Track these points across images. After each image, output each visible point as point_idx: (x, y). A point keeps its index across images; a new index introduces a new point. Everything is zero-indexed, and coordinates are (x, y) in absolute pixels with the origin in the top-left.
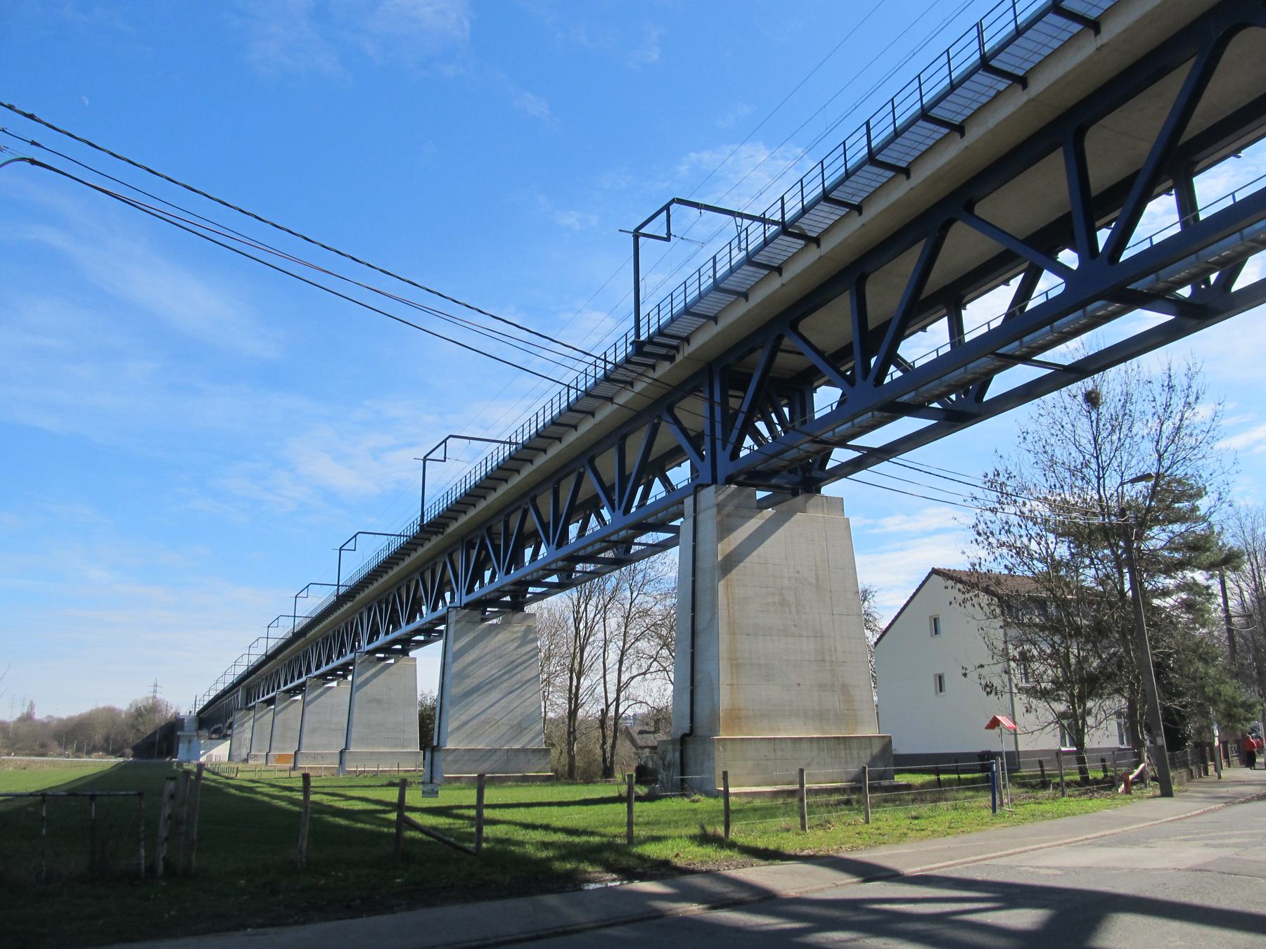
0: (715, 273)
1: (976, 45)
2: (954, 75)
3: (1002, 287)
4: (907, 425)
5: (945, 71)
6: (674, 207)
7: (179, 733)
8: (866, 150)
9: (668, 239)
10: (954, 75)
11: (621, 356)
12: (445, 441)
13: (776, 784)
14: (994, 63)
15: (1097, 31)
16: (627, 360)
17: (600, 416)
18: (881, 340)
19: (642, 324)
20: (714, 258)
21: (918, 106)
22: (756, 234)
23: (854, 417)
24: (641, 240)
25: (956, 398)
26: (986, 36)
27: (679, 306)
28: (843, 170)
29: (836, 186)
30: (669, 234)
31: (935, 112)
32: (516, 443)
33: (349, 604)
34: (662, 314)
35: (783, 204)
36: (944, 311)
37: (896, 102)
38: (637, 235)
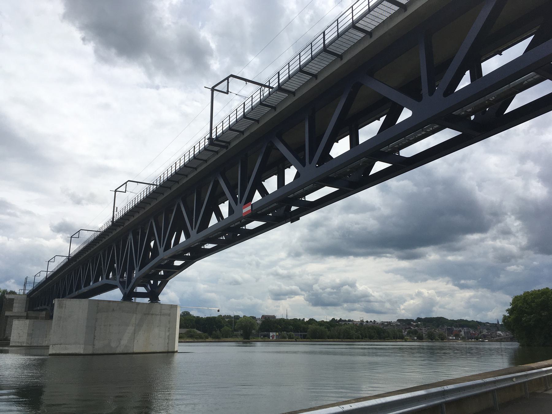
0: (279, 80)
1: (277, 80)
2: (354, 18)
3: (377, 121)
4: (327, 190)
5: (336, 29)
6: (230, 79)
7: (7, 313)
8: (322, 45)
9: (227, 93)
10: (354, 18)
11: (202, 146)
12: (126, 183)
13: (34, 356)
14: (357, 25)
15: (316, 78)
16: (205, 149)
17: (166, 195)
18: (442, 71)
19: (213, 131)
20: (244, 103)
21: (351, 21)
22: (266, 91)
23: (306, 184)
24: (215, 92)
25: (352, 178)
26: (326, 37)
27: (295, 67)
28: (336, 34)
29: (285, 82)
30: (228, 91)
31: (305, 69)
32: (156, 185)
33: (74, 263)
34: (302, 59)
35: (279, 76)
36: (348, 132)
37: (231, 116)
38: (213, 89)
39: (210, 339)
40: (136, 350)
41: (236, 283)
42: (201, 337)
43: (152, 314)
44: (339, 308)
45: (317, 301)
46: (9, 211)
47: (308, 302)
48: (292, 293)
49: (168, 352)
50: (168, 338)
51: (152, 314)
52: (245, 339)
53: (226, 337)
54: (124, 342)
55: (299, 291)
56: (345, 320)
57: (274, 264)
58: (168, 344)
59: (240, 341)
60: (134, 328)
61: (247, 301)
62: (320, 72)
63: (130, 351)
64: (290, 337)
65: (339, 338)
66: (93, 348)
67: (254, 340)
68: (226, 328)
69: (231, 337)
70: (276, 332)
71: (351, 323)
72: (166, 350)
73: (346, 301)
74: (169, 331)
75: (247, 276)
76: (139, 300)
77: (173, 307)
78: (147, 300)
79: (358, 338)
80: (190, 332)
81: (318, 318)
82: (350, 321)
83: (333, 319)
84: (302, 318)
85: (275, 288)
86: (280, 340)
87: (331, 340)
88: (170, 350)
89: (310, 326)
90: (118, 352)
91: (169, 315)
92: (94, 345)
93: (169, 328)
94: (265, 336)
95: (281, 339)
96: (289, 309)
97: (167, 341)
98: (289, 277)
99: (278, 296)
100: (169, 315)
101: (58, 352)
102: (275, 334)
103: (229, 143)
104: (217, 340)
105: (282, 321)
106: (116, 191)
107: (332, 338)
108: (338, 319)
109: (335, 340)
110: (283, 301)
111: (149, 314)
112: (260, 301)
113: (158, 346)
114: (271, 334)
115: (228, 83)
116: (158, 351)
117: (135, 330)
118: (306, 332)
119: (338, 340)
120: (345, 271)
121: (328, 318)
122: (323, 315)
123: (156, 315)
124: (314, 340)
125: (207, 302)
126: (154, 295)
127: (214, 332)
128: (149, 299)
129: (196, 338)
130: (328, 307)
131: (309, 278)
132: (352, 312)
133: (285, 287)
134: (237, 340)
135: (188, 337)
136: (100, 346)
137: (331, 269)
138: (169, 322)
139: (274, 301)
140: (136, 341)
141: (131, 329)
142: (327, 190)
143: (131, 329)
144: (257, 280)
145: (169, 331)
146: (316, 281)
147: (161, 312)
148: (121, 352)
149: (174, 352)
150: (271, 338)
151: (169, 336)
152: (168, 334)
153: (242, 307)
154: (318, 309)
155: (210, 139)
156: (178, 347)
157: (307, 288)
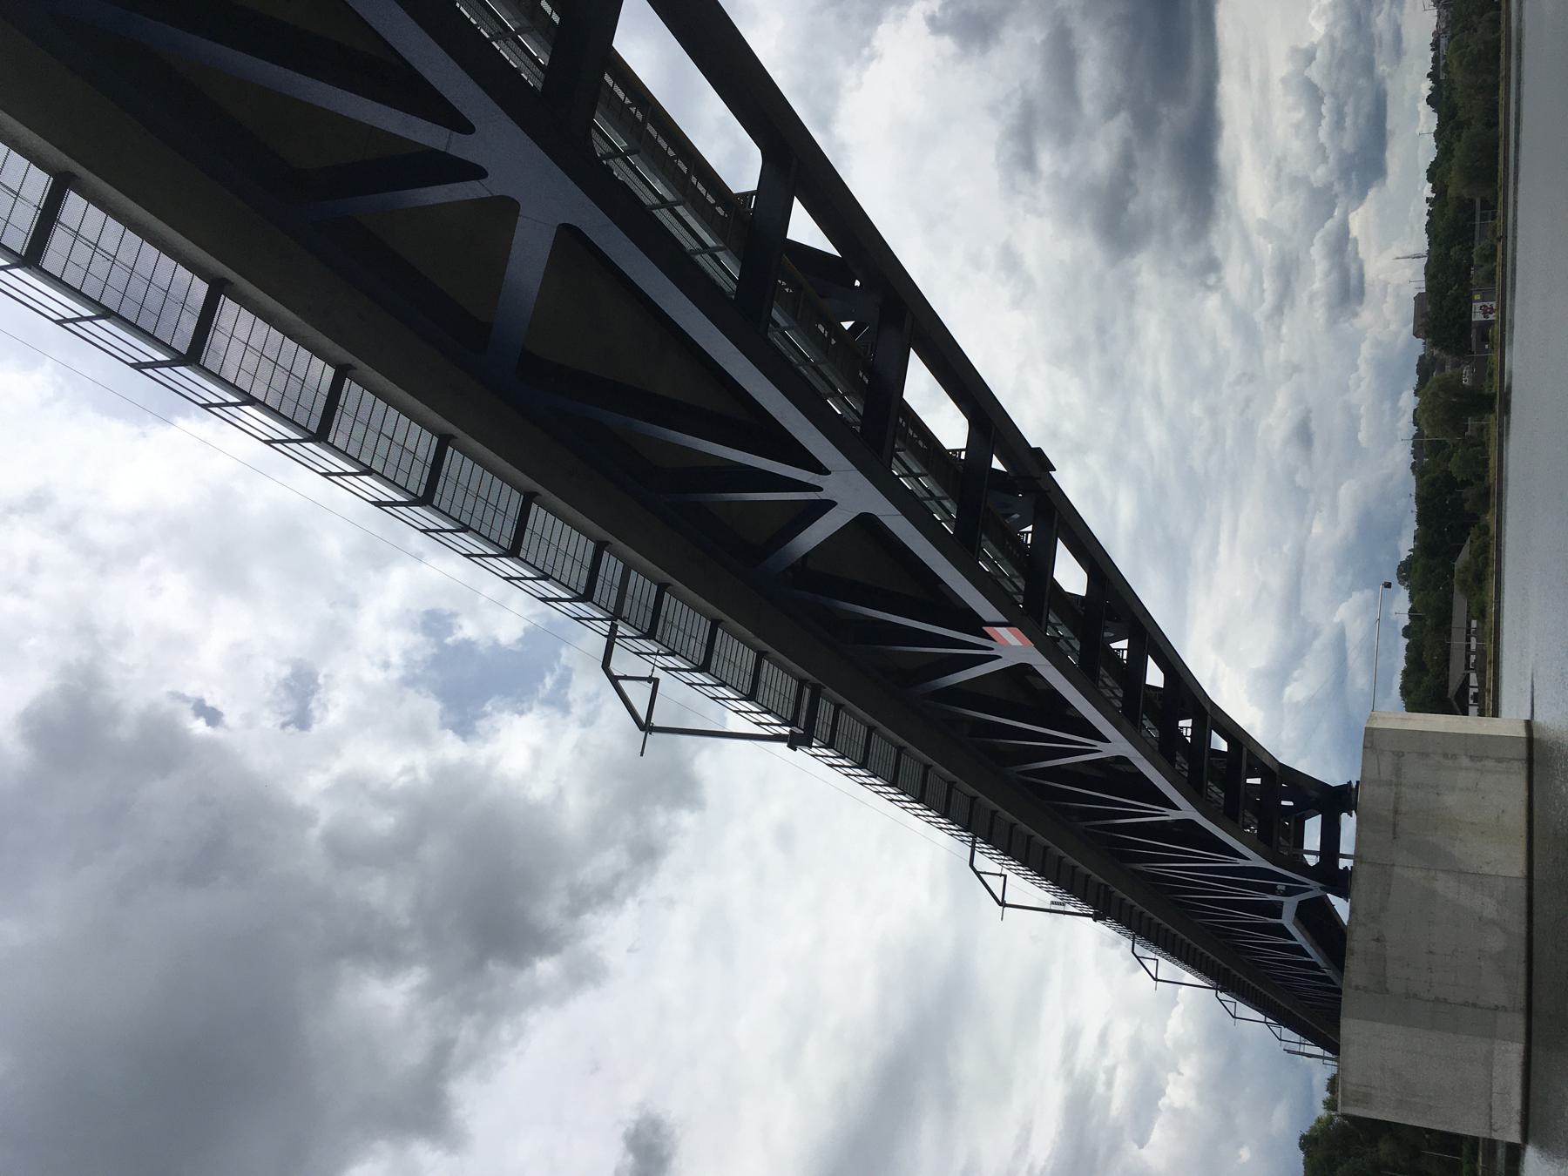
4: (921, 389)
39: (1490, 518)
40: (1518, 869)
41: (1303, 435)
42: (1485, 549)
43: (1396, 812)
44: (1390, 86)
45: (1365, 165)
46: (1100, 1089)
47: (1372, 193)
48: (1341, 244)
49: (1530, 760)
50: (1480, 759)
51: (1396, 812)
52: (1492, 410)
53: (1485, 463)
54: (1490, 909)
55: (1329, 224)
56: (1435, 60)
57: (1242, 323)
58: (1499, 760)
59: (1501, 426)
60: (1440, 875)
61: (1363, 387)
62: (514, 486)
63: (1521, 886)
64: (1490, 256)
65: (1496, 87)
66: (1505, 1009)
67: (1497, 378)
68: (1453, 467)
69: (1483, 445)
70: (1470, 301)
71: (1443, 41)
72: (1520, 770)
73: (1368, 66)
74: (1454, 757)
75: (1281, 400)
76: (1347, 844)
77: (1373, 740)
78: (1348, 823)
79: (1496, 22)
80: (1464, 582)
81: (1428, 151)
82: (1435, 45)
83: (1430, 101)
84: (1426, 207)
85: (1320, 315)
86: (1498, 289)
87: (1501, 117)
88: (1522, 751)
89: (1450, 191)
90: (1521, 930)
91: (1399, 755)
92: (1497, 1008)
93: (1445, 756)
94: (1485, 338)
95: (1499, 282)
96: (1395, 251)
97: (1490, 764)
98: (1288, 271)
99: (1349, 290)
100: (1399, 755)
101: (1517, 1118)
102: (1477, 306)
103: (802, 683)
104: (1494, 500)
105: (1431, 273)
106: (1002, 904)
107: (1493, 110)
108: (1428, 83)
109: (1502, 102)
110: (1370, 273)
111: (1395, 825)
112: (1366, 350)
113: (1506, 795)
114: (1478, 317)
115: (626, 678)
116: (1523, 794)
117: (1447, 871)
118: (1472, 202)
119: (1502, 92)
120: (1265, 87)
121: (1428, 120)
122: (1415, 134)
123: (1398, 798)
124: (1501, 174)
125: (1369, 529)
126: (1332, 801)
127: (1467, 506)
128: (1344, 816)
129: (1486, 563)
130: (1389, 126)
131: (1291, 206)
132: (1404, 45)
133: (1318, 275)
134: (1494, 431)
135: (1481, 589)
136: (1504, 989)
137: (1260, 132)
138: (1424, 755)
139: (1367, 298)
140: (1487, 869)
141: (1445, 885)
142: (921, 389)
143: (1445, 885)
144: (1297, 368)
145: (1454, 757)
146: (1297, 182)
147: (1390, 783)
148: (1524, 918)
149: (1530, 740)
150: (1491, 317)
151: (1472, 758)
152: (1465, 762)
153: (1387, 405)
154: (1395, 158)
155: (793, 742)
156: (1508, 723)
157: (1322, 202)
